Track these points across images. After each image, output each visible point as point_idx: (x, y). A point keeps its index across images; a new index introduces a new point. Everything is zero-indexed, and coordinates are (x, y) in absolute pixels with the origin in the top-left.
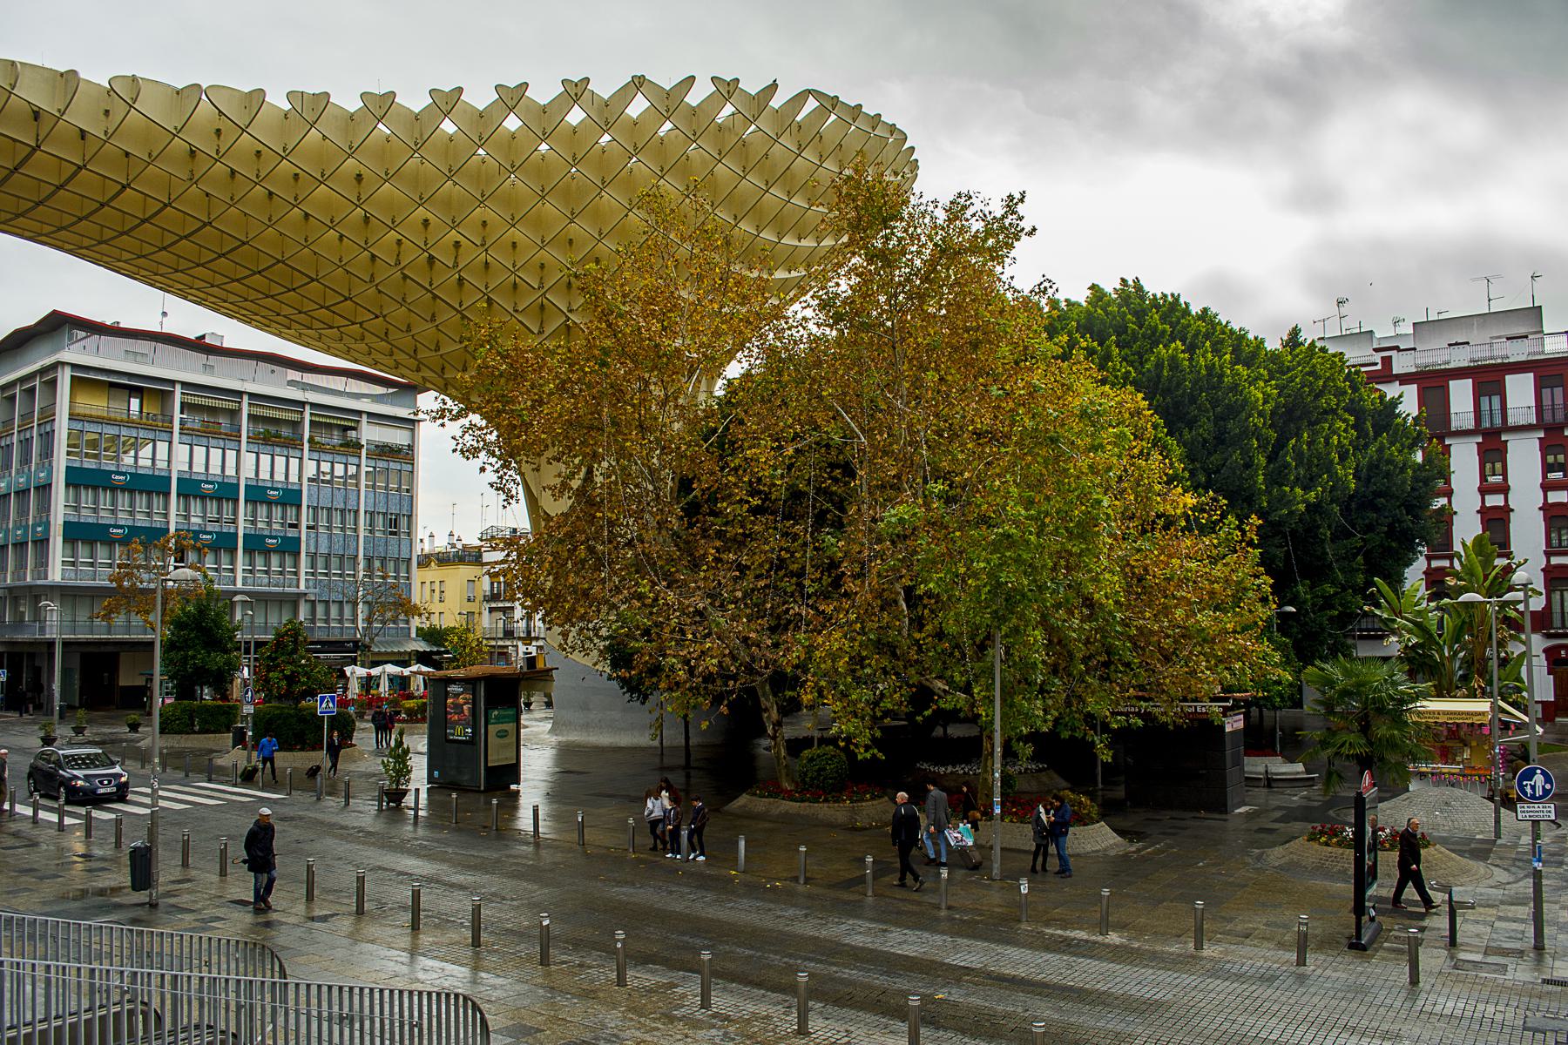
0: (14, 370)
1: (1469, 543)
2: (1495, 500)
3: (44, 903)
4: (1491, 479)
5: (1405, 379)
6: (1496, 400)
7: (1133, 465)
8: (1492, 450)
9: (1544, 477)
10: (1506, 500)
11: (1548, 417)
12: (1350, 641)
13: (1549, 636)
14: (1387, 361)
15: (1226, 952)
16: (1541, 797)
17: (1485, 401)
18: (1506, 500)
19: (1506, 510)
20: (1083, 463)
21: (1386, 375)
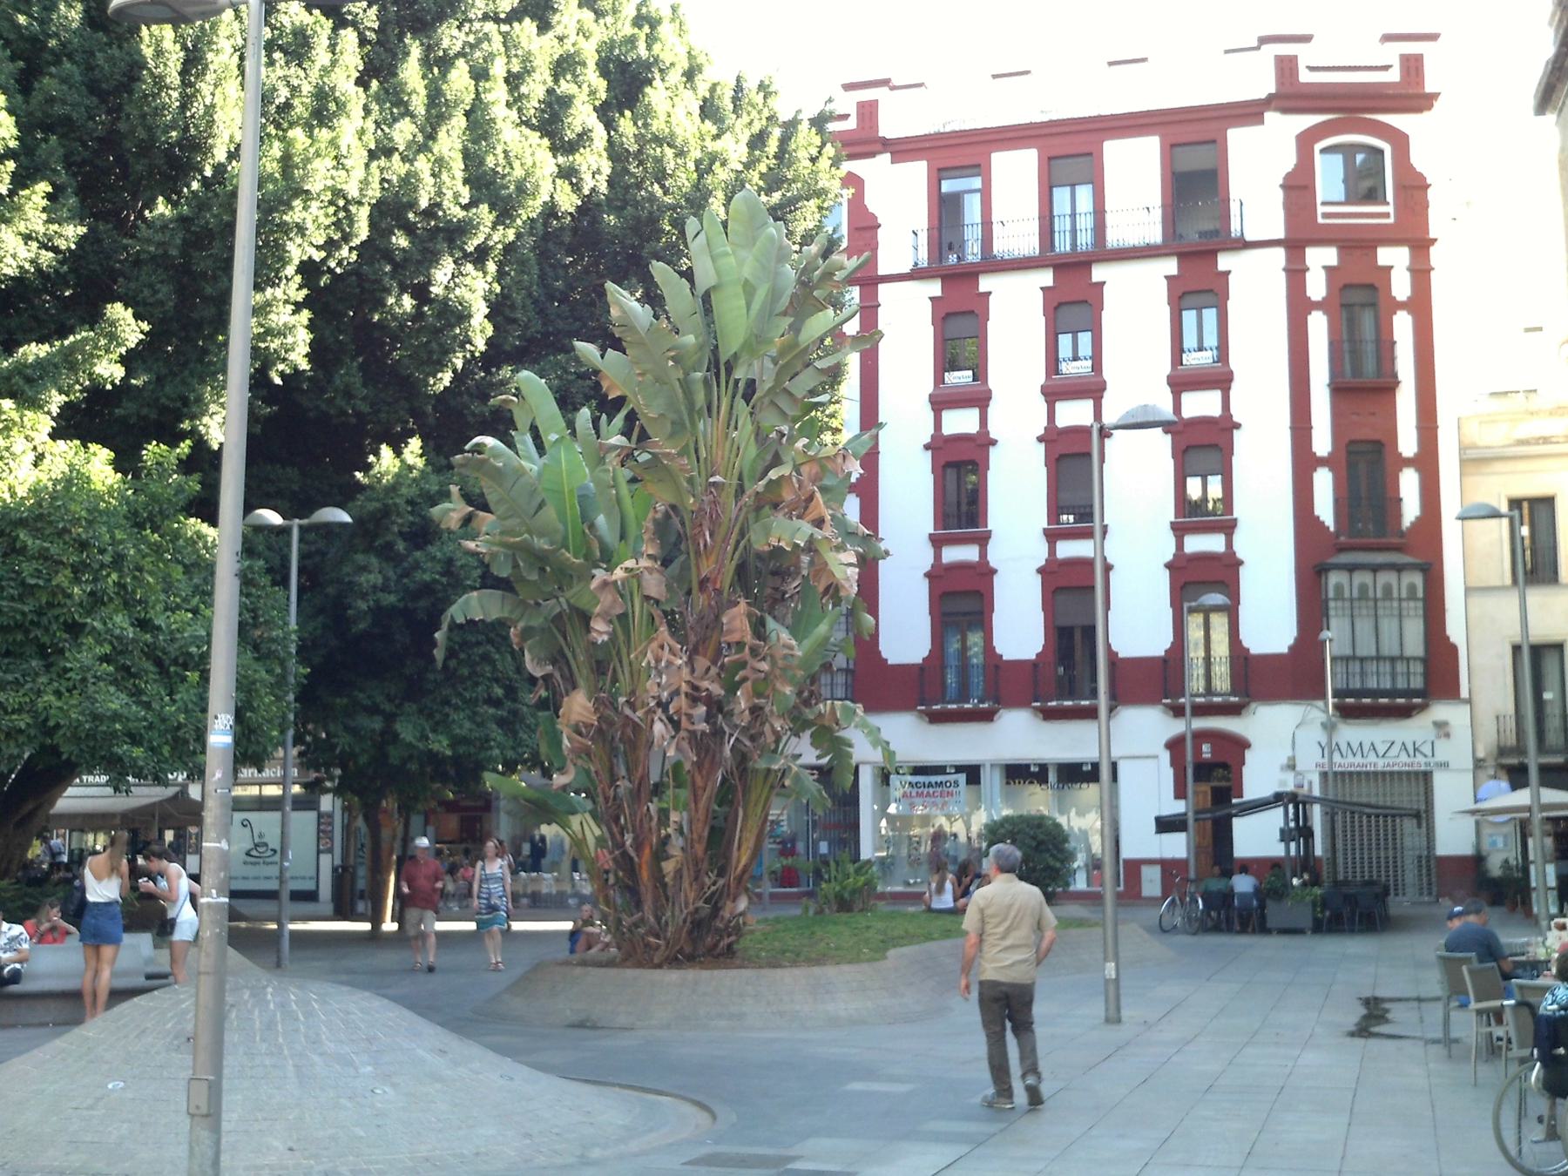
0: (1323, 830)
1: (818, 752)
2: (961, 422)
3: (1419, 826)
4: (1068, 368)
5: (903, 149)
6: (1084, 194)
7: (651, 711)
8: (1074, 304)
9: (939, 379)
10: (1229, 544)
11: (1062, 244)
12: (32, 732)
13: (1178, 712)
14: (868, 112)
15: (208, 955)
16: (135, 888)
17: (1061, 196)
18: (1229, 544)
19: (982, 442)
20: (1405, 798)
21: (864, 141)
